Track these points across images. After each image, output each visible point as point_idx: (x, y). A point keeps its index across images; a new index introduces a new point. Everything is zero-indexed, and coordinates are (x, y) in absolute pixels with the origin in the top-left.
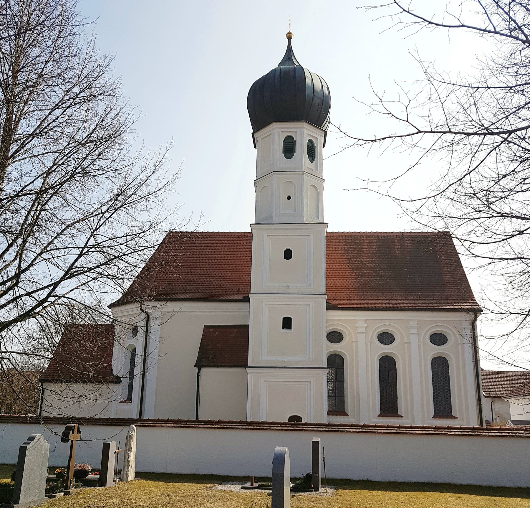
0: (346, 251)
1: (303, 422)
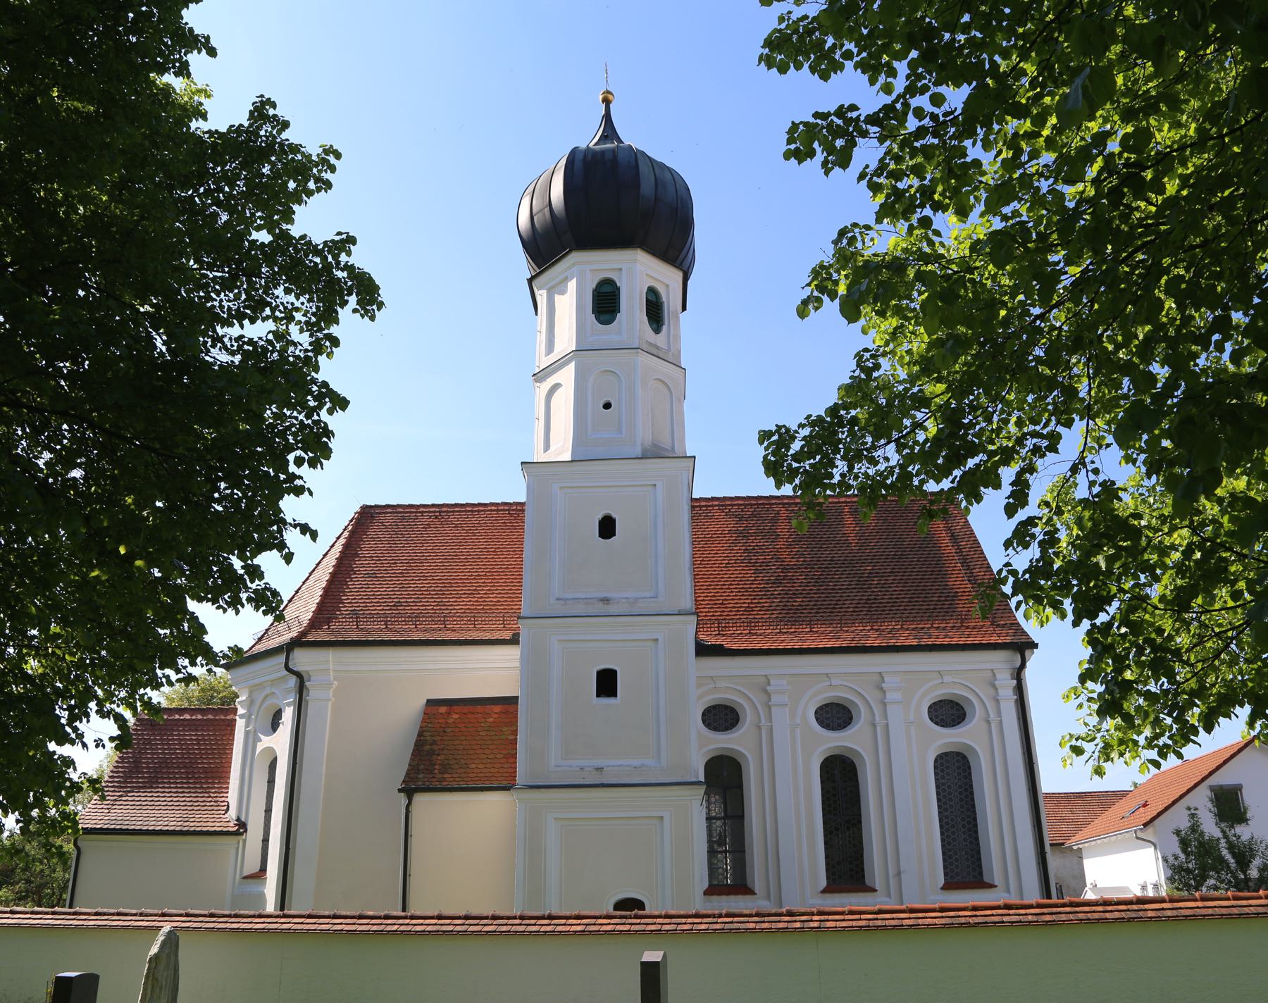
0: (744, 535)
1: (647, 911)
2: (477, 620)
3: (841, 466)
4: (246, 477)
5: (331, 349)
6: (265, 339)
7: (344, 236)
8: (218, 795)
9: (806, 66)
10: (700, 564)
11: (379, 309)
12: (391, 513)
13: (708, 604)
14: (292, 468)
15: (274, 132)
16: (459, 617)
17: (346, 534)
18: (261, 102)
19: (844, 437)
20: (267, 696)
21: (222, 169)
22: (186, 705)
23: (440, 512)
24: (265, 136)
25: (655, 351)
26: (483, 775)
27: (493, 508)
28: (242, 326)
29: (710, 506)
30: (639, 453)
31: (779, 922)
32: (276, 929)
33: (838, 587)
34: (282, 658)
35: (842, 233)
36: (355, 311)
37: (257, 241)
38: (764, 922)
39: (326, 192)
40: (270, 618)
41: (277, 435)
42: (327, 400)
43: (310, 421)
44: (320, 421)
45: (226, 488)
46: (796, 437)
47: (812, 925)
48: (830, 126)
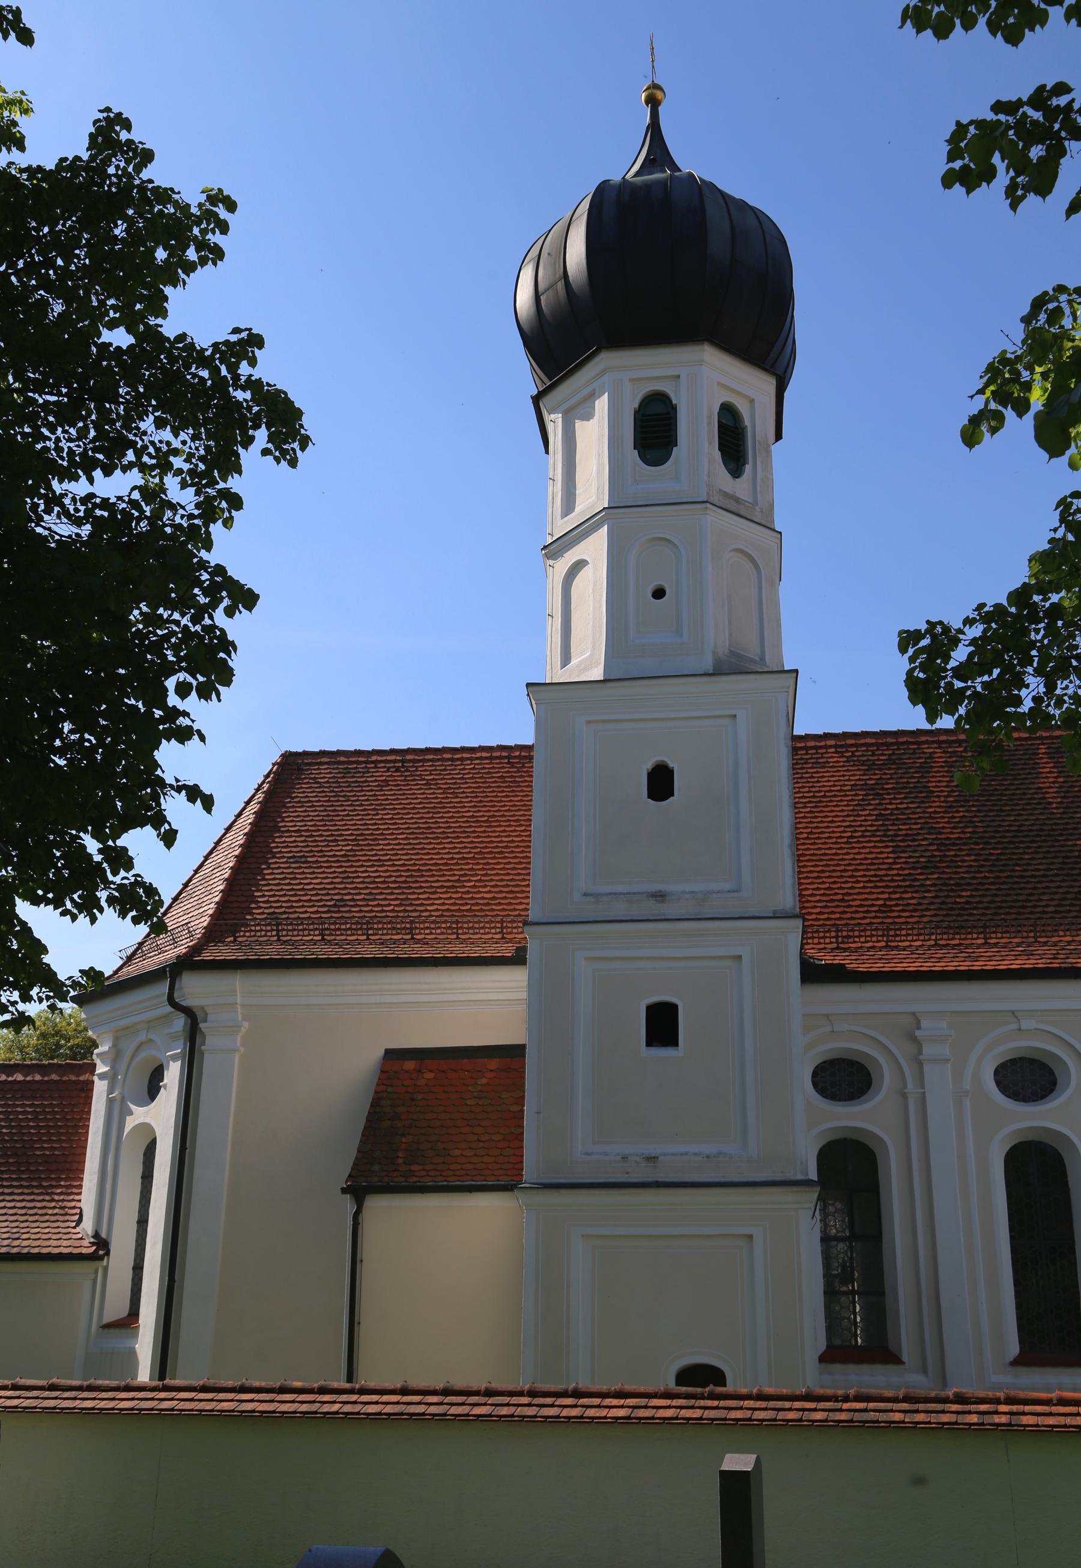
1: (729, 1388)
2: (462, 928)
3: (1035, 685)
4: (103, 715)
5: (230, 513)
6: (126, 499)
7: (244, 335)
8: (66, 1198)
9: (982, 21)
10: (807, 838)
11: (303, 448)
12: (327, 763)
13: (819, 901)
14: (173, 700)
15: (130, 169)
16: (433, 922)
17: (260, 796)
18: (107, 119)
19: (1039, 637)
20: (141, 1045)
21: (51, 230)
22: (17, 1058)
23: (403, 761)
24: (116, 175)
25: (732, 505)
26: (471, 1166)
27: (485, 755)
28: (91, 480)
29: (821, 747)
30: (708, 664)
31: (943, 1412)
32: (152, 1409)
33: (1029, 873)
34: (164, 987)
35: (1038, 303)
36: (265, 452)
37: (111, 344)
38: (917, 1411)
39: (215, 264)
40: (143, 929)
41: (150, 649)
42: (224, 594)
43: (198, 628)
44: (213, 627)
45: (71, 732)
46: (960, 640)
47: (997, 1419)
48: (1020, 124)
